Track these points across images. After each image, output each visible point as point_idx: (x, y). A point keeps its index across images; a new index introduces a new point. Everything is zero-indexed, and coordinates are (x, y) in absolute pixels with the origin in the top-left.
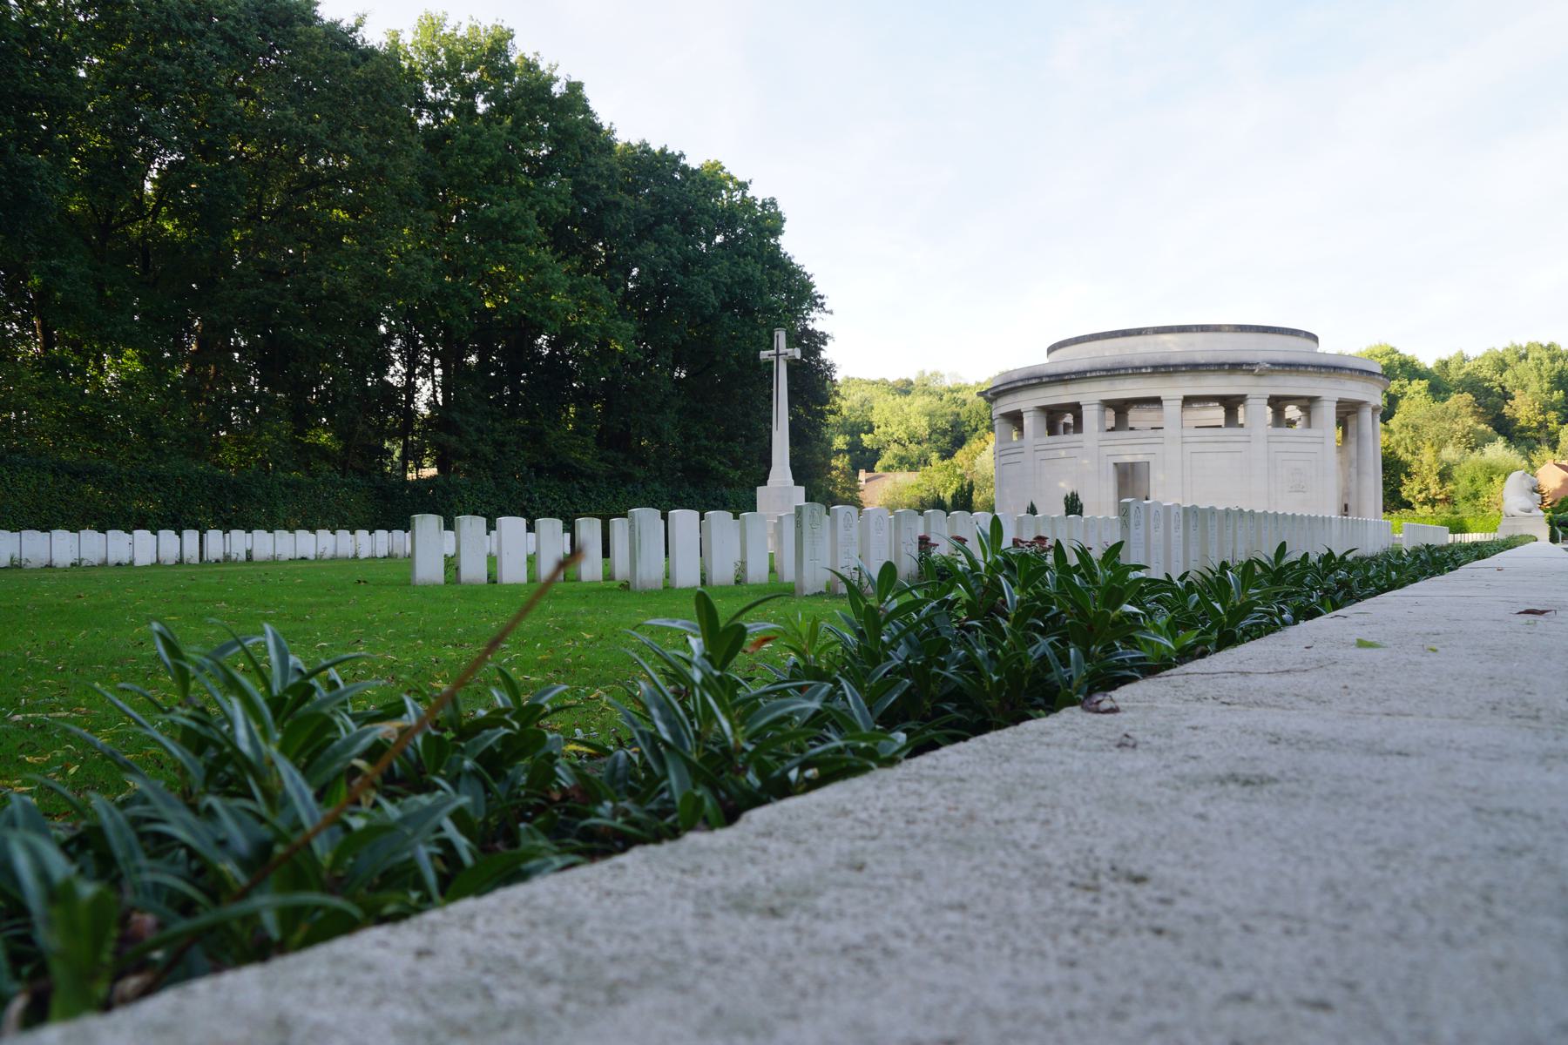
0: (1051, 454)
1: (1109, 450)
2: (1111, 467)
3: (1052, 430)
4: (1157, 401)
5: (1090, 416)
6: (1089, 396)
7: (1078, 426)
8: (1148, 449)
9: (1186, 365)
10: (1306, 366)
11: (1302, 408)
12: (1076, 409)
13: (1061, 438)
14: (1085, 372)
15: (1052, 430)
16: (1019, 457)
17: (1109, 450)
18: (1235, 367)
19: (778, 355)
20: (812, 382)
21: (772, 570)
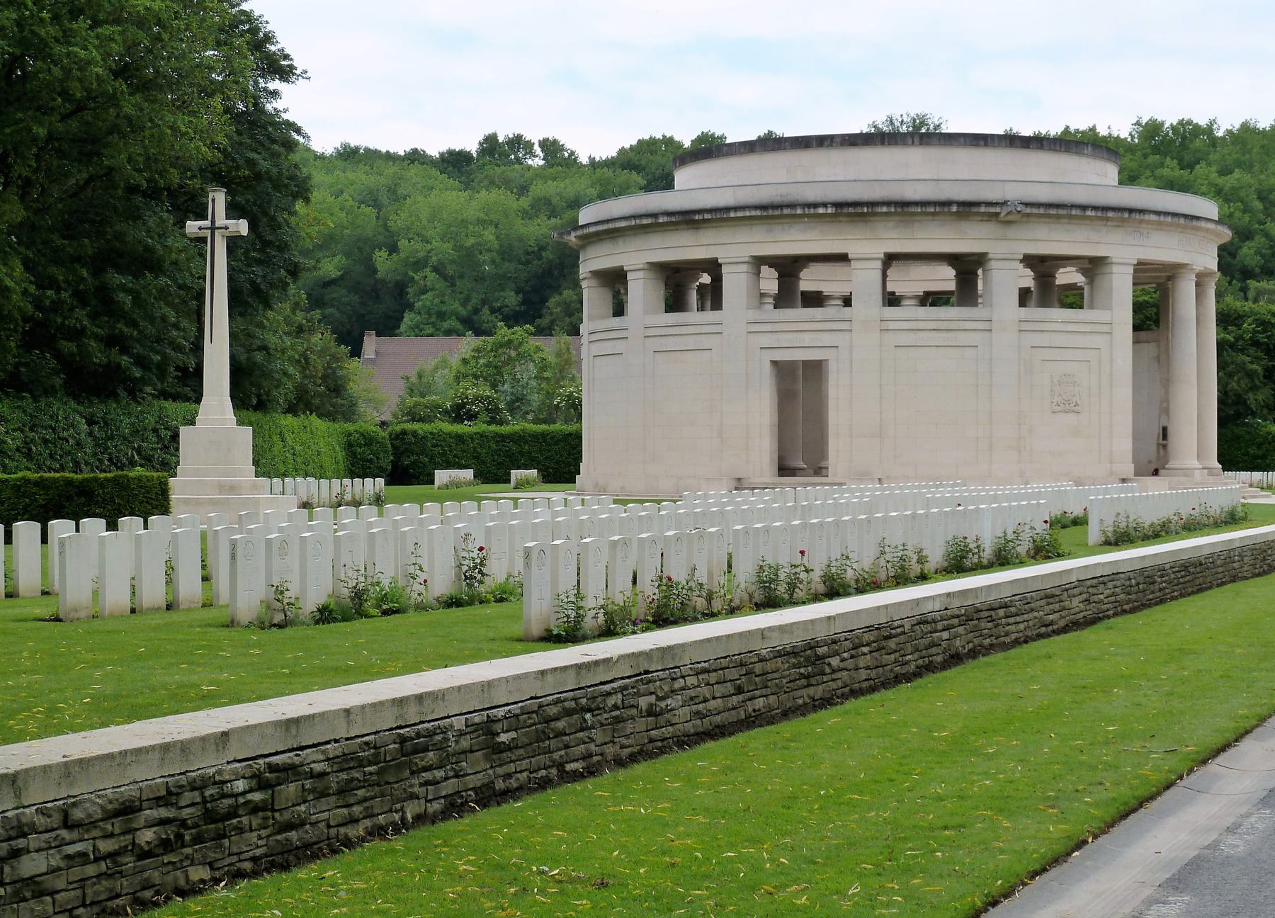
0: (670, 344)
1: (766, 340)
2: (768, 366)
3: (675, 303)
4: (843, 258)
5: (735, 283)
6: (733, 249)
7: (713, 297)
8: (827, 339)
9: (888, 203)
10: (1084, 208)
11: (1084, 272)
12: (713, 267)
13: (693, 316)
14: (727, 209)
15: (675, 303)
16: (619, 346)
17: (766, 340)
18: (966, 210)
19: (213, 229)
20: (263, 164)
21: (95, 593)
